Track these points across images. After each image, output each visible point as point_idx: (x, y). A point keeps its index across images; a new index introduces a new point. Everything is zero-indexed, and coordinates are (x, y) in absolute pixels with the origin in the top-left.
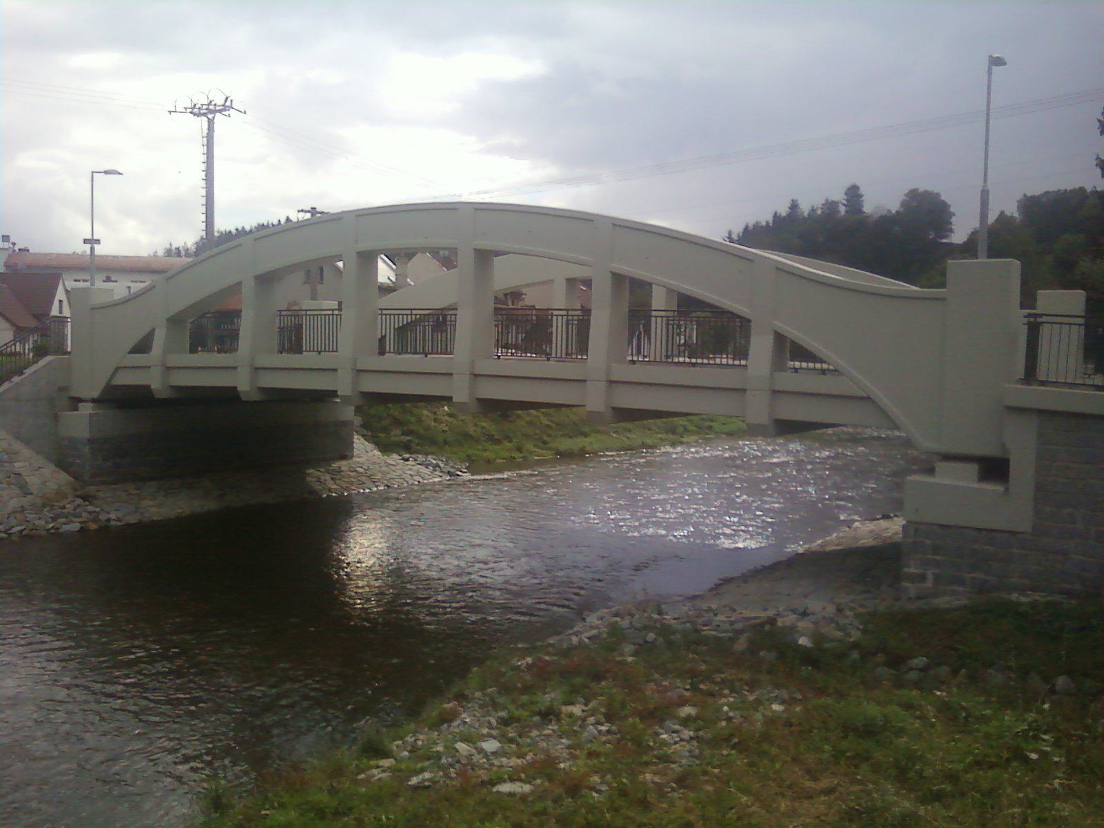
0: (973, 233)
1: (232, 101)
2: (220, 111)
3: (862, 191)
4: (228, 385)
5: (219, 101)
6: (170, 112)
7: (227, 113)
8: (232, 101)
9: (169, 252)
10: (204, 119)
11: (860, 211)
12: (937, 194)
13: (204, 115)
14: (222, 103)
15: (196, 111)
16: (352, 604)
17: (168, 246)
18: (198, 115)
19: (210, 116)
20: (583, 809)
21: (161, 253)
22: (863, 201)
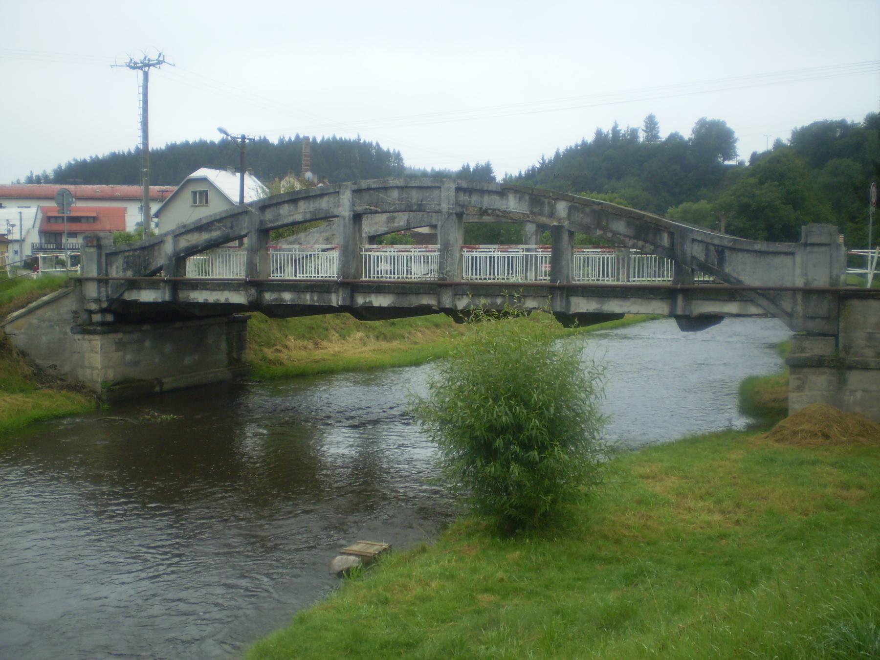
0: (767, 241)
1: (164, 56)
2: (154, 65)
3: (657, 119)
4: (712, 327)
5: (154, 57)
6: (112, 66)
7: (158, 66)
8: (164, 56)
9: (30, 180)
10: (140, 73)
11: (656, 137)
12: (723, 121)
13: (140, 68)
14: (157, 58)
15: (134, 66)
16: (547, 428)
17: (29, 175)
18: (134, 68)
19: (147, 69)
20: (842, 236)
21: (23, 180)
22: (658, 127)
